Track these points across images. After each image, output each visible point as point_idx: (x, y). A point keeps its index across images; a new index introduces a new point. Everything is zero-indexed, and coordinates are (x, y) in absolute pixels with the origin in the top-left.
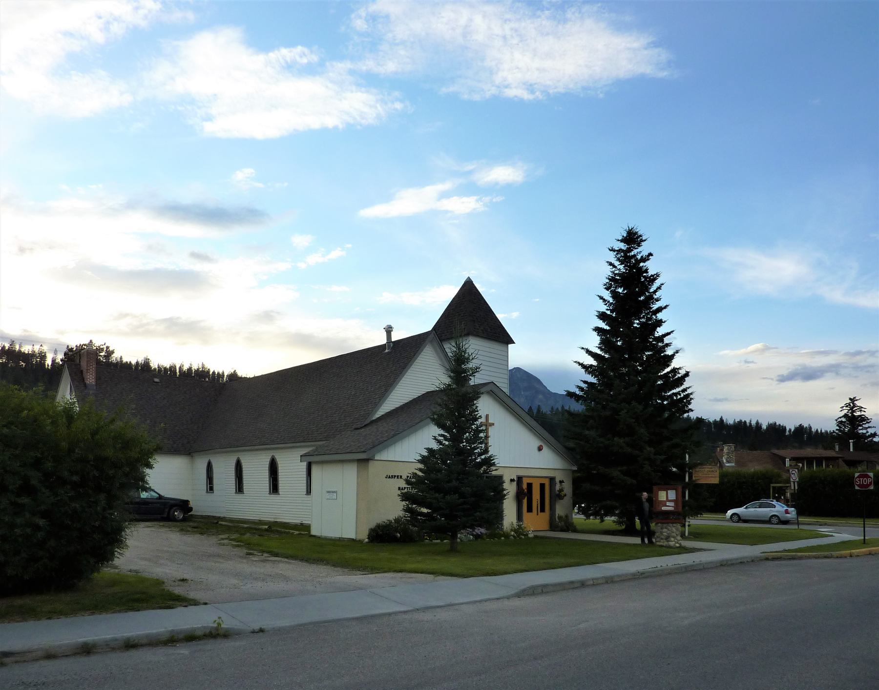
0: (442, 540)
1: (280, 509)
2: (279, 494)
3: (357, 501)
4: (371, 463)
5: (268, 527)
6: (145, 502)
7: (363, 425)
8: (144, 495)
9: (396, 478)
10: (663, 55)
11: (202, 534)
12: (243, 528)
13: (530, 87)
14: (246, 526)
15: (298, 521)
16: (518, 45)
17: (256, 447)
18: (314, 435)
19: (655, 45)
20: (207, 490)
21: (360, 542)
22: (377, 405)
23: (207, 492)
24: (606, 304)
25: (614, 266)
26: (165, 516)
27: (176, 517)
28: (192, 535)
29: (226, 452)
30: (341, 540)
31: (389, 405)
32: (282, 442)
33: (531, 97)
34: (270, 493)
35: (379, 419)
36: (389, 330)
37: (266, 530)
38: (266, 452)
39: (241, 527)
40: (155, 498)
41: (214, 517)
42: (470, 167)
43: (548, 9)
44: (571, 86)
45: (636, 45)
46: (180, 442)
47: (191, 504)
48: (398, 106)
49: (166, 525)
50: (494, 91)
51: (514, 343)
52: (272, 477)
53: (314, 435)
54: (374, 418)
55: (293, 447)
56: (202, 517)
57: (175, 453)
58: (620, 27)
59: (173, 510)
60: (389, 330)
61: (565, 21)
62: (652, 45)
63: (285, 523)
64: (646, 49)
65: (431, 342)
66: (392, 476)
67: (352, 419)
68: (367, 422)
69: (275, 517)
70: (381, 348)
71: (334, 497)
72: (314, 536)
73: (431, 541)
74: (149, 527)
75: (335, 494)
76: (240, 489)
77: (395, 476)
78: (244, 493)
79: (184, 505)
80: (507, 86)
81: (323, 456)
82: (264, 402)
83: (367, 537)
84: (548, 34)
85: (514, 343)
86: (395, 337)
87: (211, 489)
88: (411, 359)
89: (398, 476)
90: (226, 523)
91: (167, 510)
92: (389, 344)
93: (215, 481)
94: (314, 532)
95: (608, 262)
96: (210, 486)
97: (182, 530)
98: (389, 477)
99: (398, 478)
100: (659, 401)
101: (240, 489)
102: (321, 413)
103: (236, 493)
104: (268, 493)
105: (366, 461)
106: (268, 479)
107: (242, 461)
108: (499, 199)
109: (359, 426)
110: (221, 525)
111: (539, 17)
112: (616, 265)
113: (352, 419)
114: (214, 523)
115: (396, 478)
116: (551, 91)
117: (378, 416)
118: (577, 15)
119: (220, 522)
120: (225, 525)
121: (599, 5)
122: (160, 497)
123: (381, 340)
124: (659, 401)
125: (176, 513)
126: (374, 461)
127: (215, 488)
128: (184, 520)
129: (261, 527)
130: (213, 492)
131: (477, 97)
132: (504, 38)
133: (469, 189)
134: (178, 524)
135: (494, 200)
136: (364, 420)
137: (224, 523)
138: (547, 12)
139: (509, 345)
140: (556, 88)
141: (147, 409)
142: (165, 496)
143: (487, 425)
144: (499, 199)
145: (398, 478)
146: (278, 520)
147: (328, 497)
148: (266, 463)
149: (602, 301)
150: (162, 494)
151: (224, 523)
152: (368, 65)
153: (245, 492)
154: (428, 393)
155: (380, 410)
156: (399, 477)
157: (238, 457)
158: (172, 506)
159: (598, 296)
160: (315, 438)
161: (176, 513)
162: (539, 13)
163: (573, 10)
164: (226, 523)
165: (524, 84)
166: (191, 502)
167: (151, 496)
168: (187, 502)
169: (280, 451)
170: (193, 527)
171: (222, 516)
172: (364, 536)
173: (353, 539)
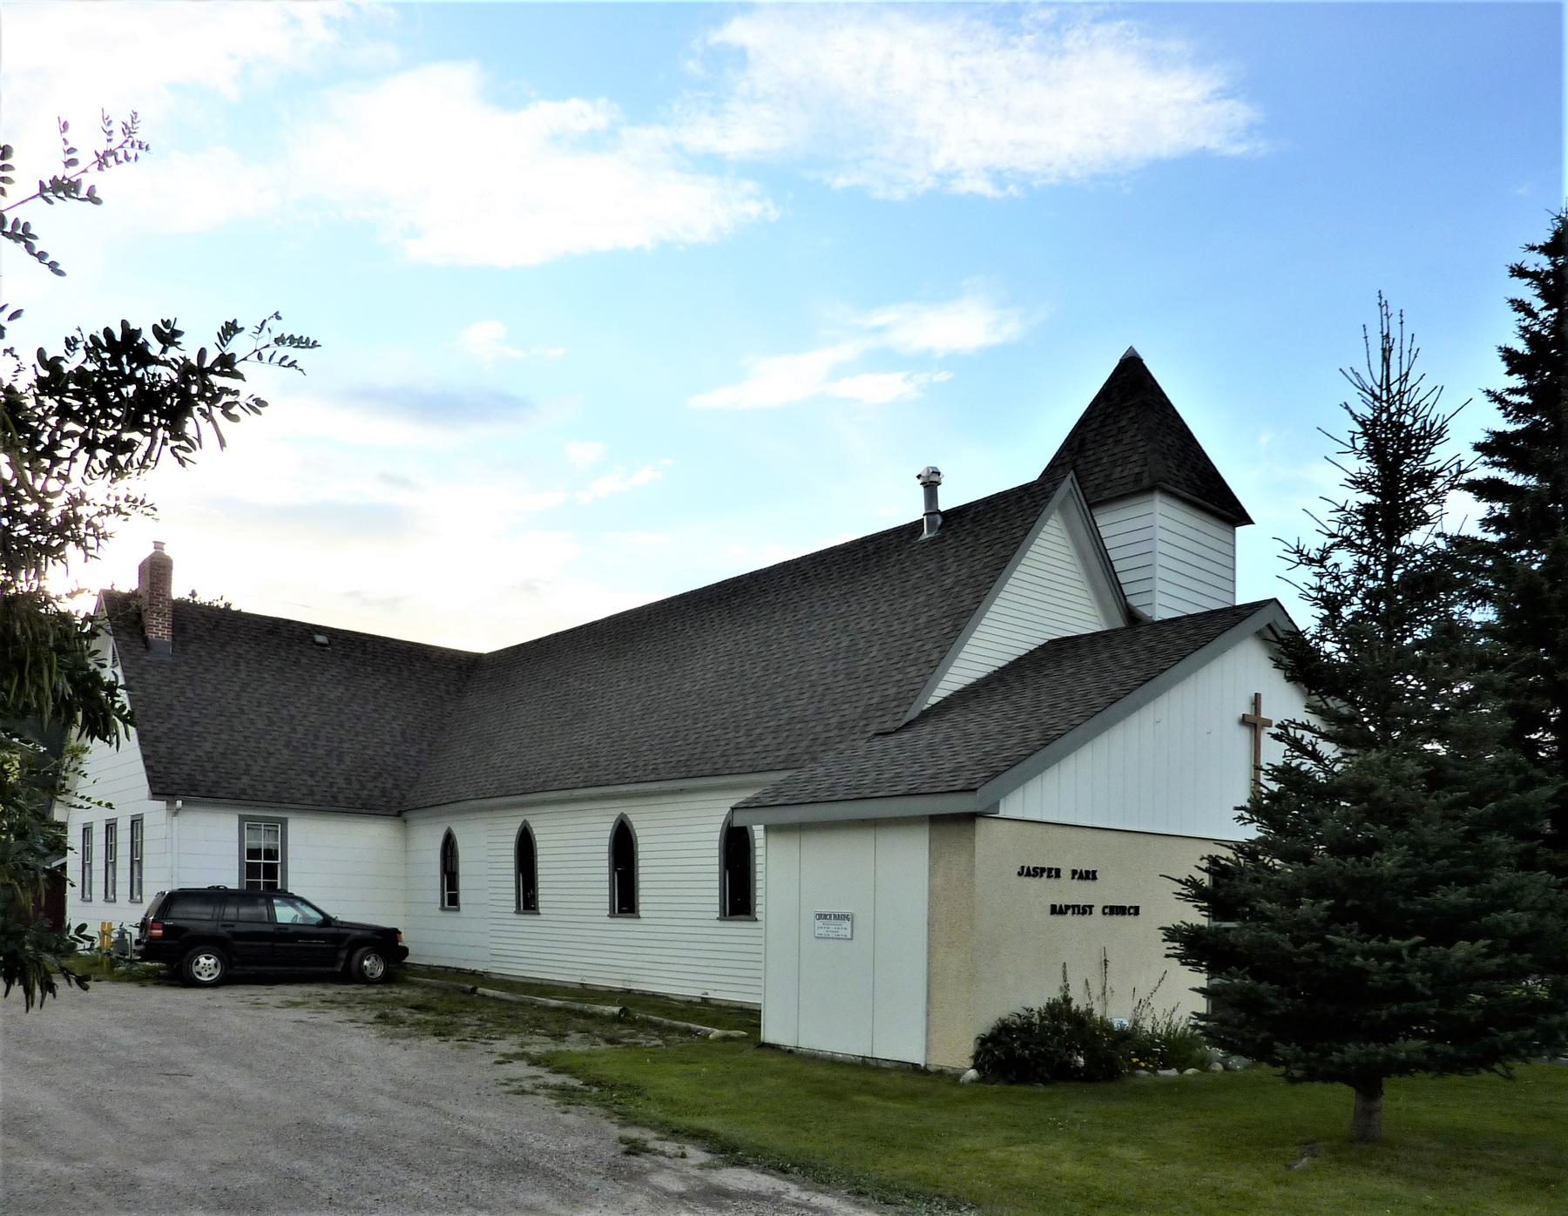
0: (1181, 1071)
1: (640, 958)
2: (539, 914)
3: (929, 945)
4: (982, 826)
5: (621, 1011)
6: (288, 934)
7: (903, 723)
8: (285, 914)
9: (1045, 874)
10: (1240, 112)
11: (440, 1034)
12: (547, 1009)
13: (998, 177)
14: (553, 1003)
15: (693, 991)
16: (976, 98)
17: (576, 793)
18: (747, 757)
19: (1224, 94)
20: (443, 903)
21: (953, 1078)
22: (935, 664)
23: (443, 908)
24: (1506, 415)
25: (1531, 314)
26: (339, 970)
27: (368, 973)
28: (415, 1041)
29: (492, 809)
30: (866, 1066)
31: (962, 671)
32: (652, 777)
33: (998, 194)
34: (612, 915)
35: (925, 715)
36: (931, 484)
37: (615, 1019)
38: (606, 805)
39: (539, 1007)
40: (314, 923)
41: (460, 972)
42: (880, 318)
43: (1030, 33)
44: (1073, 173)
45: (1191, 95)
46: (376, 787)
47: (406, 940)
48: (753, 208)
49: (340, 998)
50: (930, 183)
51: (1251, 522)
52: (619, 873)
53: (747, 757)
54: (933, 700)
55: (681, 791)
56: (432, 971)
57: (364, 811)
58: (1157, 62)
59: (358, 955)
60: (931, 484)
61: (1063, 53)
62: (1219, 95)
63: (654, 995)
64: (1207, 102)
65: (1062, 507)
66: (1035, 869)
67: (859, 710)
68: (913, 713)
69: (625, 977)
70: (915, 527)
71: (842, 932)
72: (774, 1047)
73: (1154, 1071)
74: (295, 1004)
75: (847, 924)
76: (528, 900)
77: (1043, 870)
78: (539, 914)
79: (386, 942)
80: (956, 175)
81: (811, 808)
82: (584, 686)
83: (972, 1062)
84: (1030, 77)
85: (1251, 522)
86: (946, 502)
87: (451, 899)
88: (1018, 544)
89: (1050, 870)
90: (497, 993)
91: (343, 955)
92: (931, 517)
93: (464, 883)
94: (772, 1032)
95: (1512, 301)
96: (449, 895)
97: (383, 1018)
98: (1028, 874)
99: (1049, 877)
100: (1421, 722)
101: (528, 900)
102: (752, 700)
103: (518, 912)
104: (514, 909)
105: (969, 819)
106: (607, 877)
107: (535, 831)
108: (943, 377)
109: (889, 726)
110: (484, 996)
111: (1014, 46)
112: (1536, 311)
113: (859, 710)
114: (464, 992)
115: (1045, 874)
116: (1035, 184)
117: (945, 694)
118: (1082, 42)
119: (481, 990)
120: (494, 998)
121: (1123, 23)
122: (327, 921)
123: (909, 509)
124: (1421, 722)
125: (366, 963)
126: (995, 823)
127: (462, 899)
128: (388, 979)
129: (599, 1008)
130: (458, 910)
131: (899, 194)
132: (952, 85)
133: (886, 360)
134: (371, 991)
135: (935, 379)
136: (902, 709)
137: (490, 992)
138: (1028, 38)
139: (1237, 529)
140: (1045, 176)
141: (298, 705)
142: (340, 919)
143: (1255, 725)
144: (943, 377)
145: (1049, 877)
146: (633, 987)
147: (823, 932)
148: (600, 842)
149: (1497, 405)
150: (332, 912)
151: (490, 992)
152: (703, 135)
153: (541, 911)
154: (1054, 644)
155: (942, 685)
156: (1053, 873)
157: (525, 821)
158: (358, 943)
159: (1489, 392)
160: (749, 763)
161: (366, 963)
162: (1014, 39)
163: (1076, 33)
164: (497, 993)
165: (987, 170)
166: (403, 935)
167: (305, 917)
168: (394, 933)
169: (651, 801)
170: (412, 1007)
171: (480, 968)
172: (958, 1055)
173: (916, 1066)
